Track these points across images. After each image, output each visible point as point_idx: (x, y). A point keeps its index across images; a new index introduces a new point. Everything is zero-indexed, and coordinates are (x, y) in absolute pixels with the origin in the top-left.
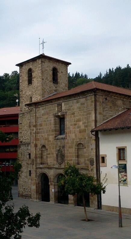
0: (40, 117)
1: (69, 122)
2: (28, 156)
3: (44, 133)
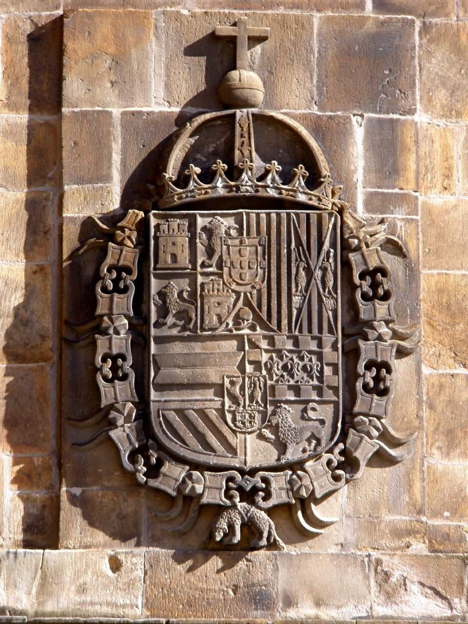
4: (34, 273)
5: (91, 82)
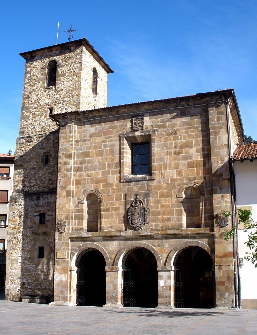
0: (85, 140)
1: (163, 149)
2: (37, 219)
3: (94, 169)
4: (125, 212)
5: (128, 198)
